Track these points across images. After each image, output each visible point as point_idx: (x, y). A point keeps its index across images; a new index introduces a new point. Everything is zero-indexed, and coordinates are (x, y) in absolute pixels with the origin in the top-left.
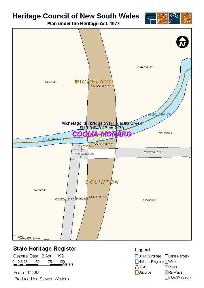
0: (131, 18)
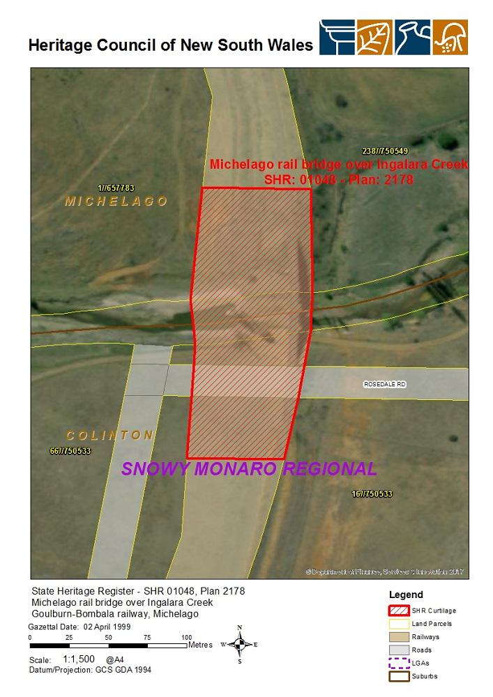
0: (293, 50)
